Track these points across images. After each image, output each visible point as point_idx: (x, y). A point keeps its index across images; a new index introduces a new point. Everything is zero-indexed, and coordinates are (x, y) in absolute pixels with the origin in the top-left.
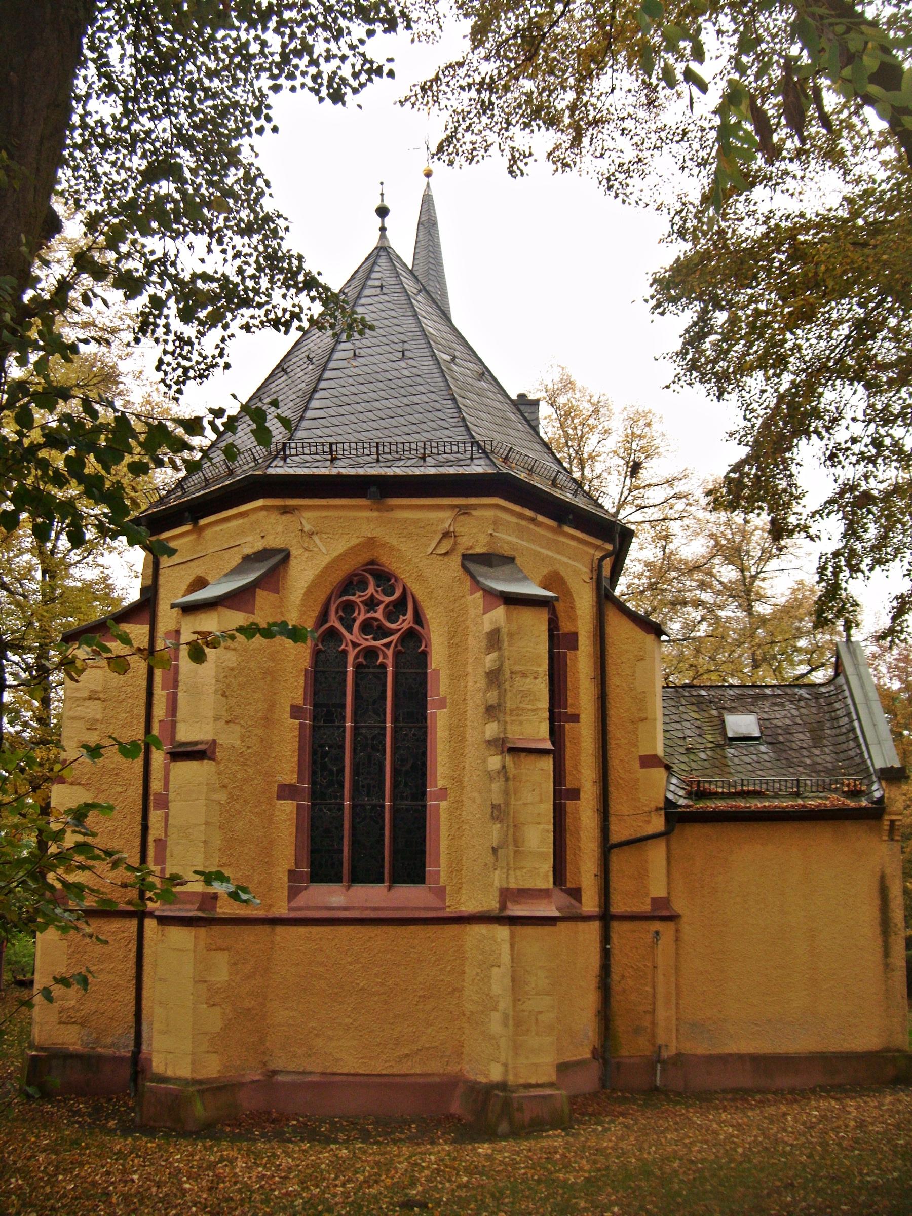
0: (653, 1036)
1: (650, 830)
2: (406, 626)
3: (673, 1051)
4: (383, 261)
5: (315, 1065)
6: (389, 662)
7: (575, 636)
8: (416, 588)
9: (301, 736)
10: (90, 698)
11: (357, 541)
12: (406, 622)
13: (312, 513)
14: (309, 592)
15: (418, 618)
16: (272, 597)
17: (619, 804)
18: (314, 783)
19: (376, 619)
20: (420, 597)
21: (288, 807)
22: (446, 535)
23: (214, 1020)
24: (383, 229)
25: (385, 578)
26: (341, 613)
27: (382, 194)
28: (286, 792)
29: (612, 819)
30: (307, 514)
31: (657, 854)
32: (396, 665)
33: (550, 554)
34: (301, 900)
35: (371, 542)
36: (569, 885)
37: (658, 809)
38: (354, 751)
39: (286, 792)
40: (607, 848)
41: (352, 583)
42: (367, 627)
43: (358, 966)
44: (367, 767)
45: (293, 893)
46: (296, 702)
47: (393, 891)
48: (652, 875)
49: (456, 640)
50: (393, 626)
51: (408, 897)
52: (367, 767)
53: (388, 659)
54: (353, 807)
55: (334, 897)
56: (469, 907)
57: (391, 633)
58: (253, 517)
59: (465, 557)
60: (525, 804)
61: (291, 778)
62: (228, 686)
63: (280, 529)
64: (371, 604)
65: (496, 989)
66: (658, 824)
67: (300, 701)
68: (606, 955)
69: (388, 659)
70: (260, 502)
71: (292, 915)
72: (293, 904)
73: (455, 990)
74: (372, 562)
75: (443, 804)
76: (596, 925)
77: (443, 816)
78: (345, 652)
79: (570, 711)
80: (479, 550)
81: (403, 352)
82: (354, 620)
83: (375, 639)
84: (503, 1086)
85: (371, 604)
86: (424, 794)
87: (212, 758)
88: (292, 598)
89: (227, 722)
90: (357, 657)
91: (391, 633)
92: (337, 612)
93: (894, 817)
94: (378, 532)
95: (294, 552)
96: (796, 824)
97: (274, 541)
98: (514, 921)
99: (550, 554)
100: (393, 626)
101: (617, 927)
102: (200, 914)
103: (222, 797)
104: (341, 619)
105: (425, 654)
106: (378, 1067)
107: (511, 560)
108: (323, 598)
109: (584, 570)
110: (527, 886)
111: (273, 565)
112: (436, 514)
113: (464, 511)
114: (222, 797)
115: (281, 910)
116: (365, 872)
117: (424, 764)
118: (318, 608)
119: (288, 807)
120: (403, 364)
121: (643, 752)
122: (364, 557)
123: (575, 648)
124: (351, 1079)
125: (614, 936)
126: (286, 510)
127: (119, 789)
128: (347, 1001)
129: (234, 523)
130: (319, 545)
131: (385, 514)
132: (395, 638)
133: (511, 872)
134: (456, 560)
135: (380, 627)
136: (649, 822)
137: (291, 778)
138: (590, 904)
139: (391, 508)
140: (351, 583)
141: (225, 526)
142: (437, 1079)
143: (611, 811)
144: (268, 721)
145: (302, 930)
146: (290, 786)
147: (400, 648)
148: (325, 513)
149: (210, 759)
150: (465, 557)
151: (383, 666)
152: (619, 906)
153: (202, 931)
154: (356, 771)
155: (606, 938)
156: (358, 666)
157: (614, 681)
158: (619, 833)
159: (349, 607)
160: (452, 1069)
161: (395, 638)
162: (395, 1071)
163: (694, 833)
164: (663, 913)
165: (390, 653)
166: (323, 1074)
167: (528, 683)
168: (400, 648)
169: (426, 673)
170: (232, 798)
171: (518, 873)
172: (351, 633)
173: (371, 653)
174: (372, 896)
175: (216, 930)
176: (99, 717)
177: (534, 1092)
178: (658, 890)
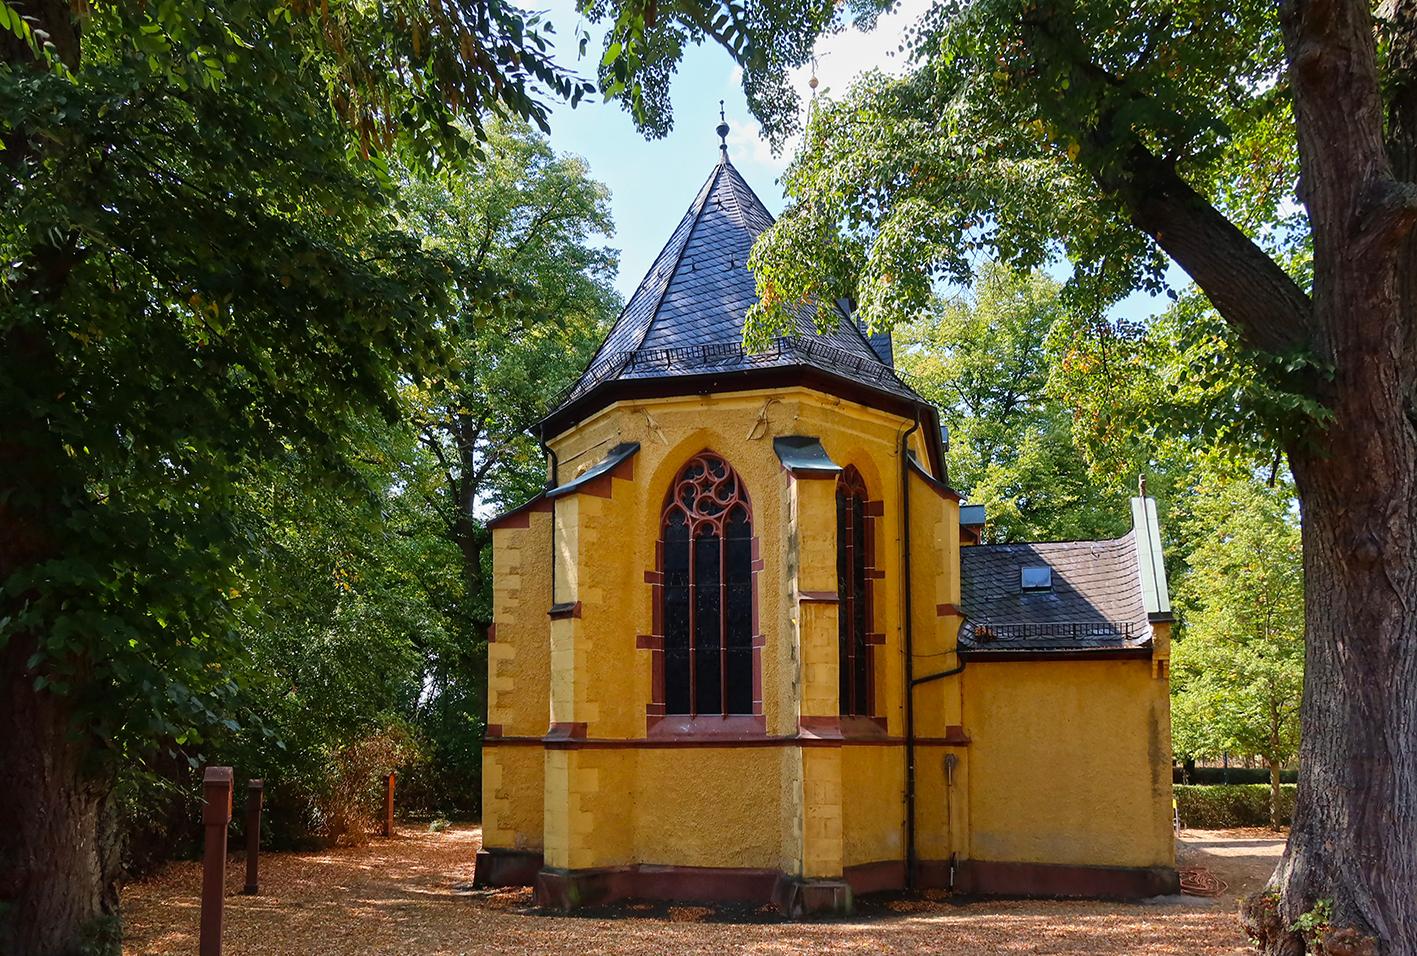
0: (950, 845)
1: (945, 668)
2: (733, 502)
3: (965, 857)
4: (726, 174)
5: (670, 860)
6: (721, 532)
7: (881, 504)
8: (739, 469)
9: (654, 596)
10: (511, 574)
11: (692, 432)
12: (733, 498)
13: (657, 409)
14: (655, 477)
15: (743, 495)
16: (627, 482)
17: (920, 647)
18: (665, 633)
19: (710, 497)
20: (743, 478)
21: (646, 654)
22: (761, 422)
23: (587, 822)
24: (724, 147)
25: (716, 462)
26: (683, 494)
27: (722, 113)
28: (644, 642)
29: (915, 660)
30: (652, 412)
31: (951, 690)
32: (726, 534)
33: (855, 433)
34: (656, 729)
35: (703, 432)
36: (877, 716)
37: (952, 651)
38: (696, 607)
39: (644, 642)
40: (911, 682)
41: (689, 469)
42: (704, 505)
43: (700, 780)
44: (707, 619)
45: (651, 722)
46: (649, 569)
47: (728, 721)
48: (948, 707)
49: (770, 512)
50: (724, 503)
51: (739, 724)
52: (707, 619)
53: (719, 530)
54: (697, 652)
55: (683, 725)
56: (782, 733)
57: (719, 509)
58: (613, 416)
59: (775, 439)
60: (815, 646)
61: (647, 631)
62: (591, 557)
63: (632, 426)
64: (706, 485)
65: (796, 800)
66: (952, 662)
67: (652, 569)
68: (910, 774)
69: (719, 530)
70: (616, 405)
71: (650, 740)
72: (653, 731)
73: (773, 800)
74: (706, 450)
75: (763, 648)
76: (901, 750)
77: (763, 657)
78: (687, 526)
79: (876, 568)
80: (787, 433)
81: (732, 262)
82: (694, 499)
83: (710, 514)
84: (800, 878)
85: (706, 485)
86: (750, 640)
87: (578, 616)
88: (643, 483)
89: (590, 587)
90: (695, 530)
91: (719, 509)
92: (679, 493)
93: (1161, 658)
94: (708, 423)
95: (644, 445)
96: (1072, 663)
97: (628, 438)
98: (804, 743)
99: (855, 433)
100: (724, 503)
101: (918, 750)
102: (571, 740)
103: (589, 645)
104: (684, 499)
105: (749, 525)
106: (719, 862)
107: (815, 441)
108: (668, 482)
109: (889, 445)
110: (818, 714)
111: (626, 457)
112: (749, 404)
113: (773, 400)
114: (589, 645)
115: (642, 734)
116: (706, 706)
117: (750, 616)
118: (665, 490)
119: (646, 654)
120: (732, 273)
121: (941, 601)
122: (700, 446)
123: (881, 514)
124: (696, 871)
125: (917, 758)
126: (635, 410)
127: (536, 645)
128: (691, 804)
129: (602, 423)
130: (664, 435)
131: (714, 407)
132: (725, 512)
133: (804, 703)
134: (769, 443)
135: (714, 504)
136: (945, 662)
137: (647, 631)
138: (895, 729)
139: (718, 401)
140: (691, 467)
141: (596, 427)
142: (760, 873)
143: (914, 653)
144: (626, 584)
145: (658, 752)
146: (645, 637)
147: (728, 520)
148: (666, 410)
149: (576, 617)
150: (775, 439)
151: (717, 536)
152: (921, 732)
153: (575, 753)
154: (697, 623)
155: (910, 760)
156: (697, 537)
157: (916, 541)
158: (919, 671)
159: (689, 488)
160: (773, 864)
161: (725, 512)
162: (729, 865)
163: (982, 670)
164: (957, 738)
165: (721, 526)
166: (676, 867)
167: (514, 582)
168: (728, 520)
169: (750, 541)
170: (596, 645)
171: (810, 703)
172: (692, 510)
173: (706, 526)
174: (712, 724)
175: (586, 751)
176: (518, 587)
177: (822, 884)
178: (952, 718)
